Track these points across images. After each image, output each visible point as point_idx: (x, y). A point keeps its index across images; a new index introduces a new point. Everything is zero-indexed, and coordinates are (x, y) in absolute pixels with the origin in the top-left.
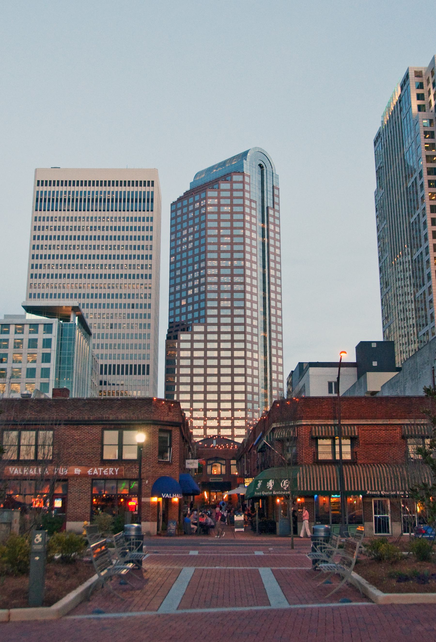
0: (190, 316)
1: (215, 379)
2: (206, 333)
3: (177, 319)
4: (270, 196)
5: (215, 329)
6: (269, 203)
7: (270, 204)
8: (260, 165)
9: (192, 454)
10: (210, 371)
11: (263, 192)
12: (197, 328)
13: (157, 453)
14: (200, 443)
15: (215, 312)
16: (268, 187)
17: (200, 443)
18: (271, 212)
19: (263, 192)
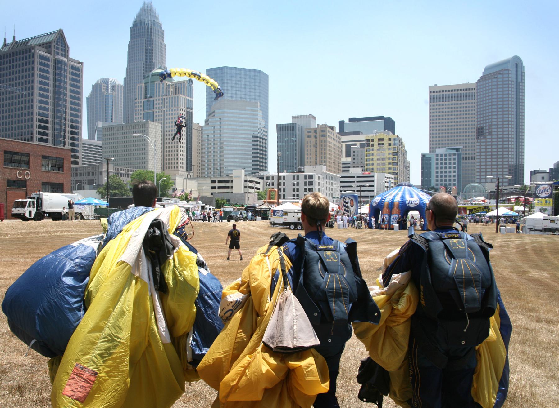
0: (484, 125)
1: (499, 143)
2: (492, 138)
3: (479, 126)
4: (520, 77)
5: (496, 137)
6: (519, 80)
7: (520, 81)
8: (517, 64)
9: (84, 355)
10: (493, 153)
11: (517, 75)
12: (488, 137)
13: (6, 184)
14: (365, 400)
15: (496, 130)
16: (519, 73)
17: (365, 400)
18: (521, 84)
19: (517, 75)
